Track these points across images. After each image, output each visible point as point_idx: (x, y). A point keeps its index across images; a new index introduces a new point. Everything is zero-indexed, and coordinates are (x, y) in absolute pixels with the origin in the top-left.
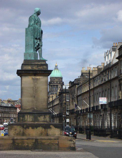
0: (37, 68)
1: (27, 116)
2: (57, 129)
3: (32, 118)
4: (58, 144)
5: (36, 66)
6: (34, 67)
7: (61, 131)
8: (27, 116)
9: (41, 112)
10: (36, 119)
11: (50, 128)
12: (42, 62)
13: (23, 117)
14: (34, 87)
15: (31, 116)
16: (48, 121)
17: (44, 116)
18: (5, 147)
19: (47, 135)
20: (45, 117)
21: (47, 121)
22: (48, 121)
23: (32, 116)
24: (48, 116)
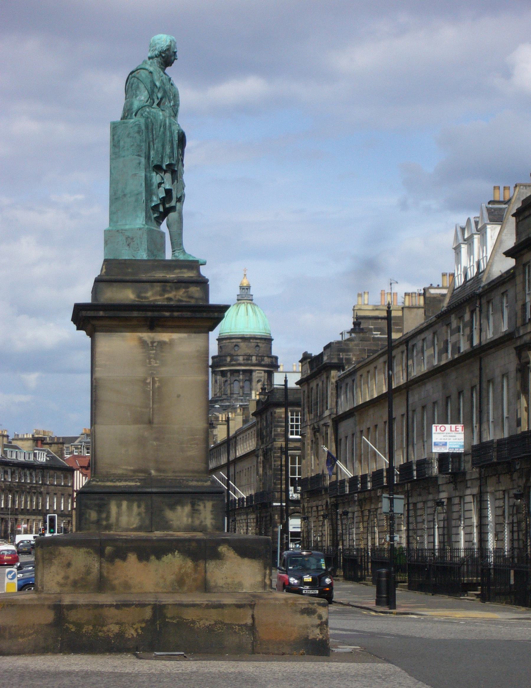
0: (161, 295)
1: (119, 506)
4: (252, 628)
8: (119, 506)
11: (217, 556)
12: (185, 271)
13: (102, 508)
14: (146, 379)
17: (193, 505)
18: (20, 640)
19: (205, 587)
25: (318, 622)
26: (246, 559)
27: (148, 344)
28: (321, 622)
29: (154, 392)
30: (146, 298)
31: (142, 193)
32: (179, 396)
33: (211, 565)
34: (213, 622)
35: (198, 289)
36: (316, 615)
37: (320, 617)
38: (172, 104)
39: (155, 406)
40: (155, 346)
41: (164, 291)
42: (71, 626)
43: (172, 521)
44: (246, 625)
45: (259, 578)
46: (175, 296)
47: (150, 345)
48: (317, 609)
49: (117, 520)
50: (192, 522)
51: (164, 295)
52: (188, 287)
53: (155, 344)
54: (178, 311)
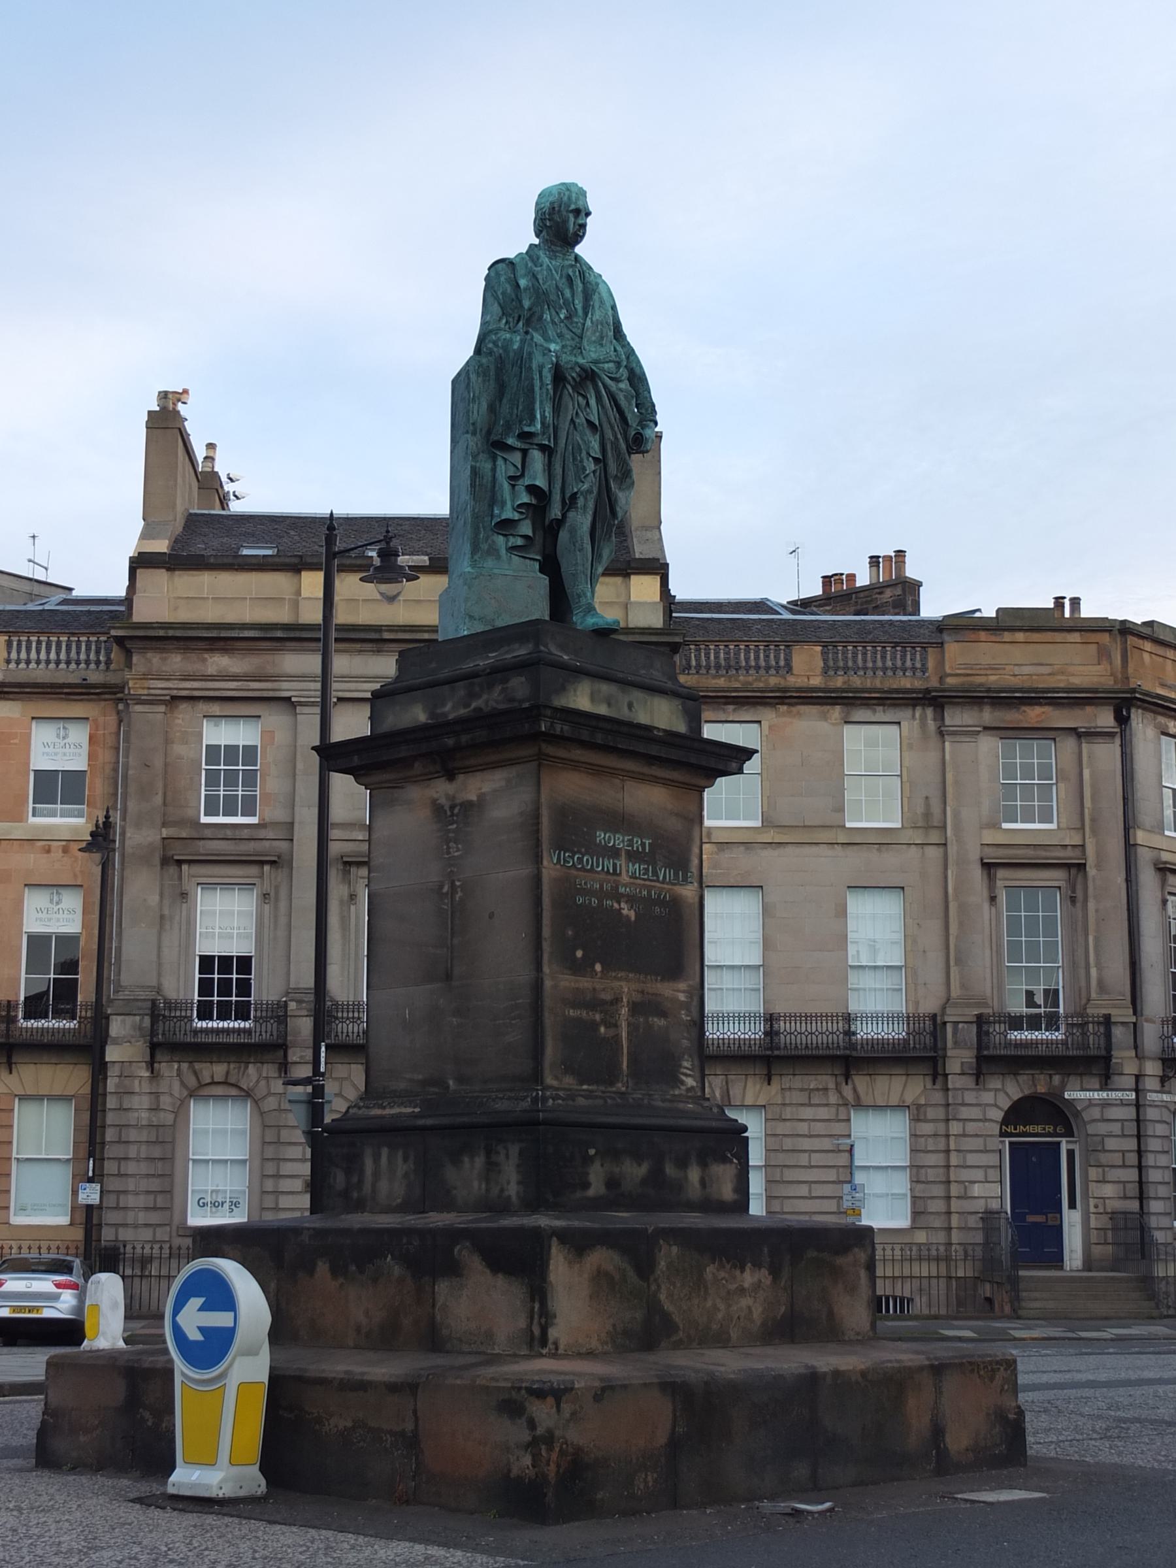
0: (467, 705)
1: (377, 1158)
2: (501, 1281)
3: (406, 1175)
4: (412, 1442)
5: (461, 690)
6: (444, 705)
7: (533, 1300)
8: (377, 1158)
9: (465, 1119)
10: (429, 1192)
11: (453, 1269)
12: (517, 646)
13: (353, 1163)
14: (441, 887)
15: (400, 1154)
16: (514, 1198)
17: (489, 1152)
18: (82, 1439)
19: (433, 1339)
20: (492, 1167)
21: (501, 1207)
22: (514, 1198)
23: (405, 1160)
24: (514, 1150)
25: (526, 1437)
26: (500, 1276)
27: (445, 812)
28: (534, 1437)
29: (453, 909)
30: (445, 715)
31: (223, 509)
32: (491, 916)
33: (442, 1288)
34: (349, 1424)
35: (523, 679)
36: (524, 1419)
37: (532, 1425)
38: (562, 316)
39: (456, 941)
40: (457, 815)
41: (472, 695)
42: (147, 1415)
43: (455, 1188)
44: (402, 1434)
45: (522, 1323)
46: (487, 702)
47: (449, 813)
48: (527, 1404)
49: (374, 1190)
50: (487, 1190)
51: (469, 706)
52: (507, 681)
53: (456, 811)
54: (644, 732)
